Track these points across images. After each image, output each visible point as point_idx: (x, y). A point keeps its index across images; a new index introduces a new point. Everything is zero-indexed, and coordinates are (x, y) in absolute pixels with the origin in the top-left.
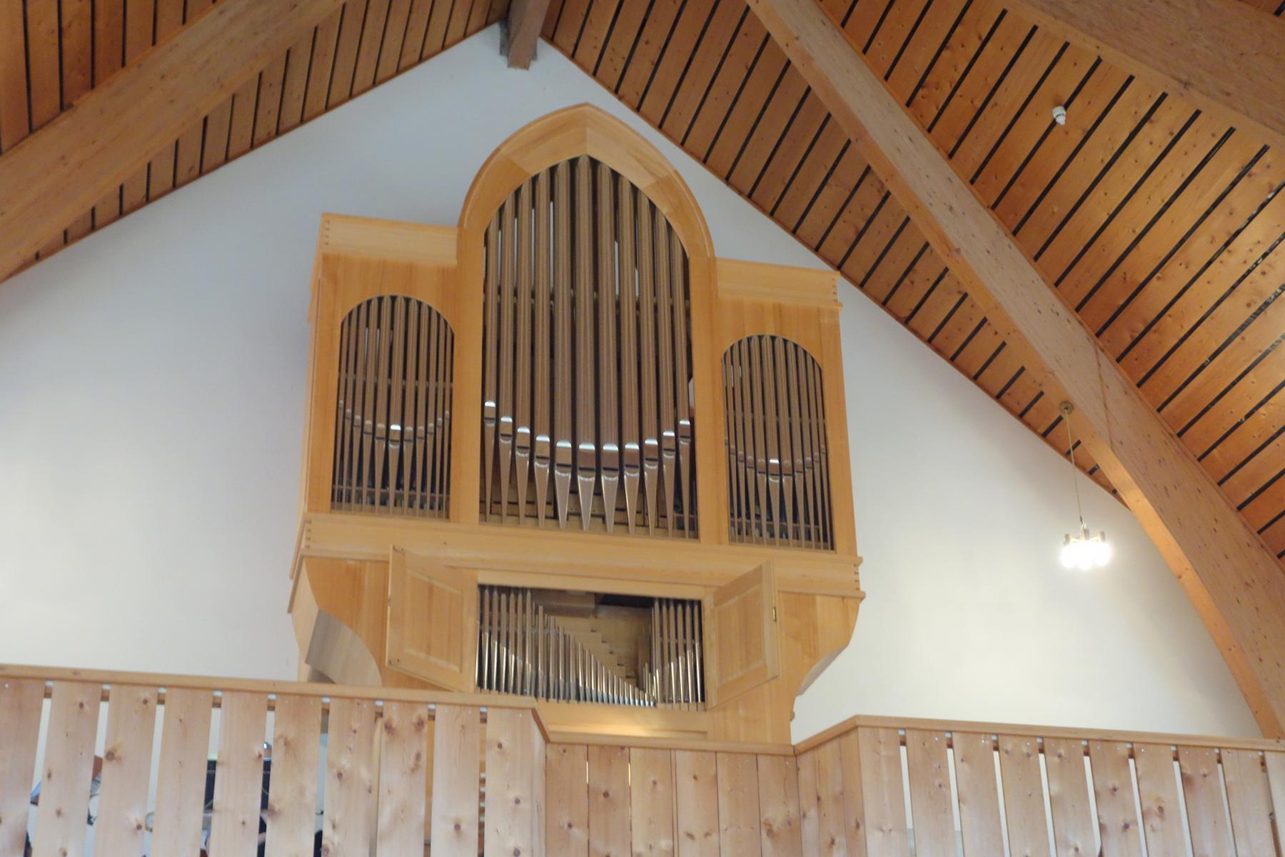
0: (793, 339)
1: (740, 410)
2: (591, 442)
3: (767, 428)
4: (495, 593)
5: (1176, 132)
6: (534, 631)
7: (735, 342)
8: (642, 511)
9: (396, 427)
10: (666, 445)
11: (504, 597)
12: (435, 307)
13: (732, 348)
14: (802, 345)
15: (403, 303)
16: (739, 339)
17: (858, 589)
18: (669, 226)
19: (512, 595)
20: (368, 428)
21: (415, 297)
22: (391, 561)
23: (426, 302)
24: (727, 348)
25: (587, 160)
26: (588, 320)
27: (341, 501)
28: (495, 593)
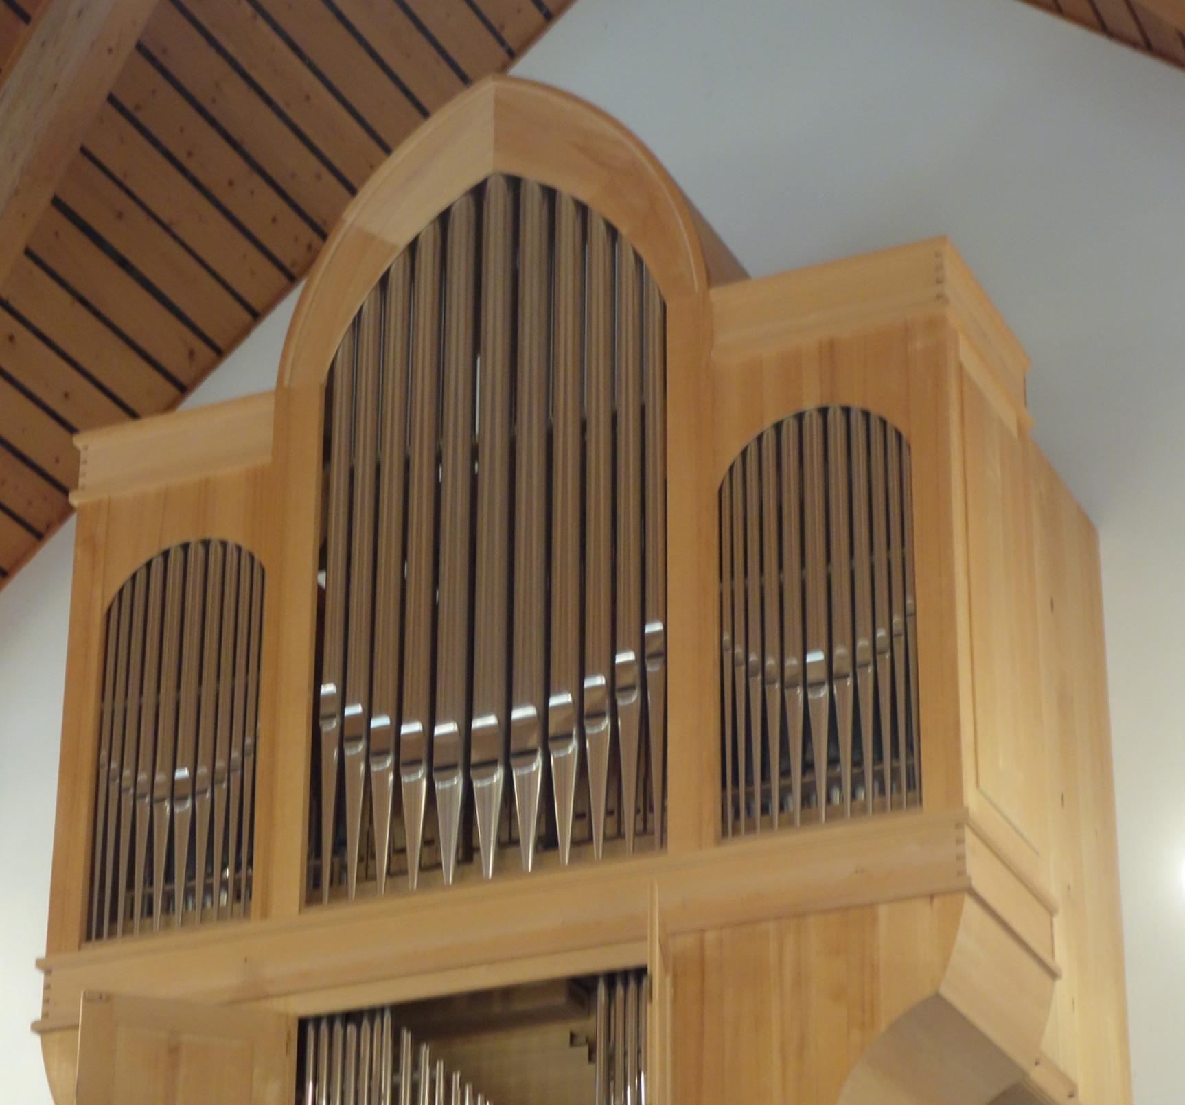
0: (856, 404)
1: (742, 575)
2: (454, 719)
3: (396, 657)
4: (338, 1027)
5: (139, 116)
6: (416, 1076)
7: (749, 439)
8: (616, 812)
9: (183, 773)
10: (623, 680)
11: (351, 1029)
12: (246, 547)
13: (744, 453)
14: (874, 410)
15: (201, 550)
16: (757, 433)
17: (962, 873)
18: (639, 260)
19: (365, 1024)
20: (127, 782)
21: (216, 535)
22: (656, 970)
23: (233, 538)
24: (734, 453)
25: (502, 182)
26: (602, 461)
27: (150, 912)
28: (338, 1027)
